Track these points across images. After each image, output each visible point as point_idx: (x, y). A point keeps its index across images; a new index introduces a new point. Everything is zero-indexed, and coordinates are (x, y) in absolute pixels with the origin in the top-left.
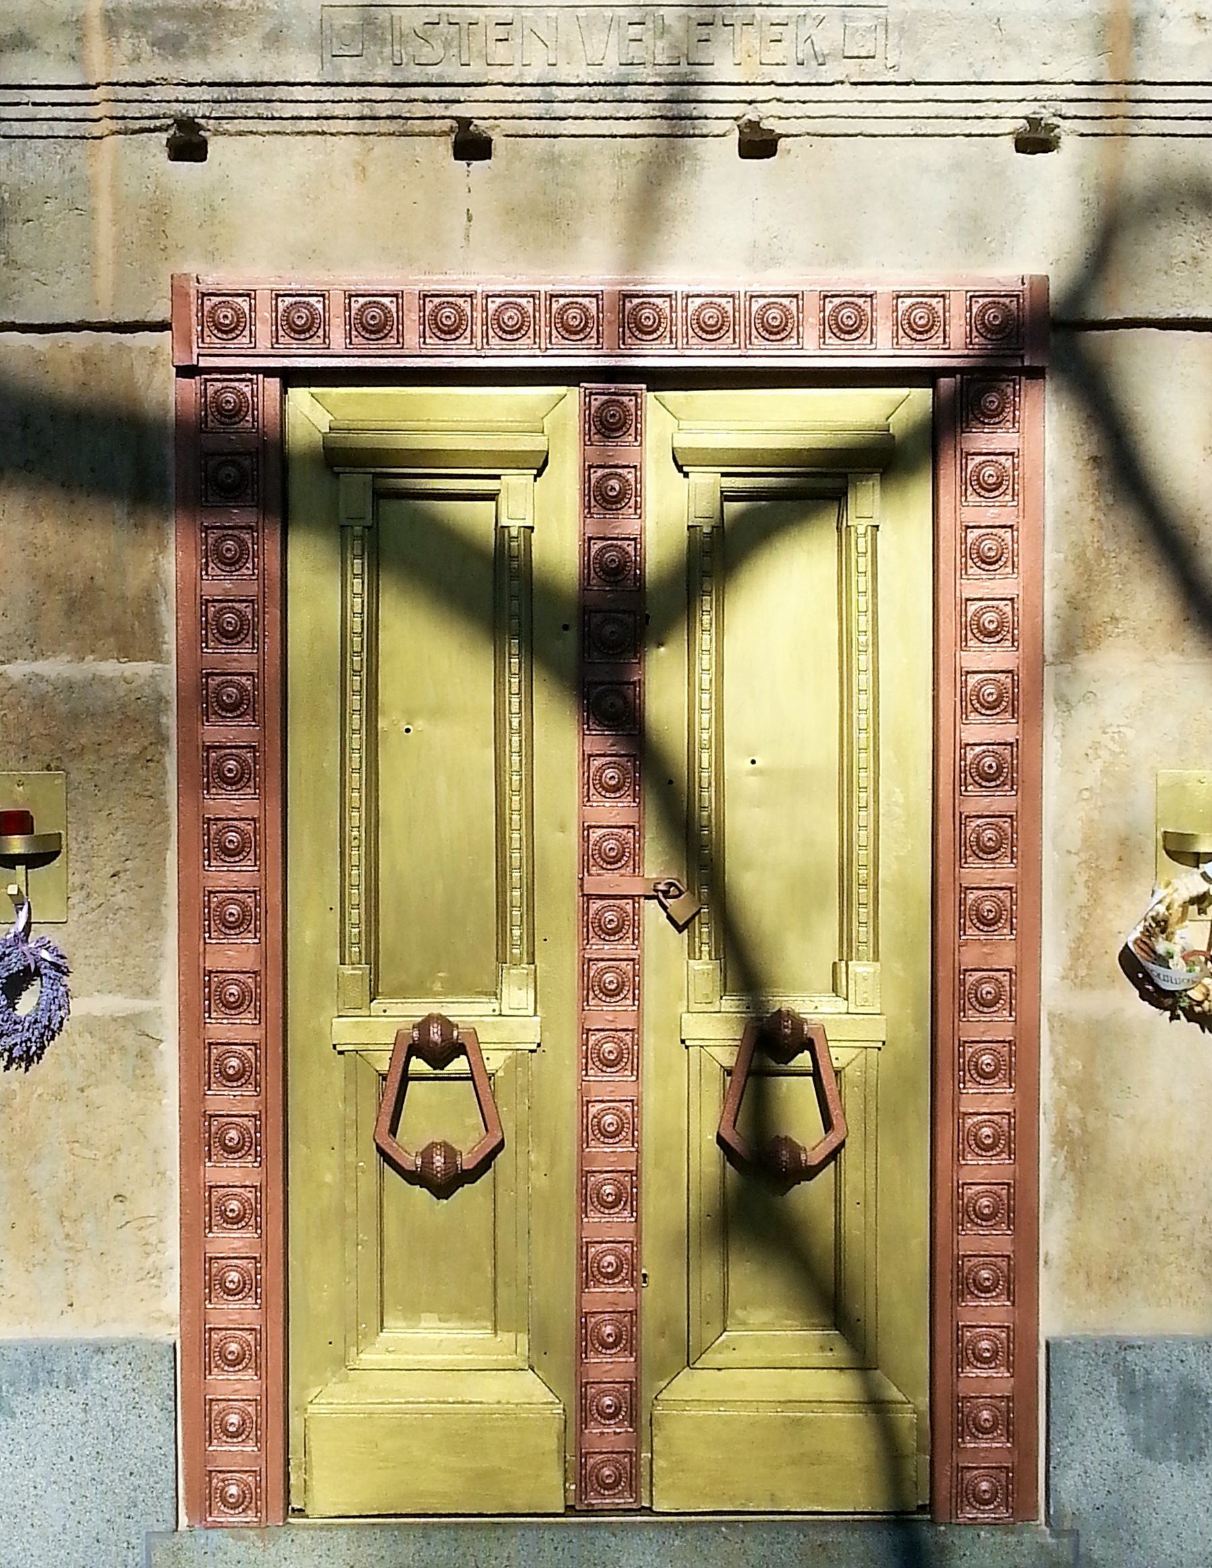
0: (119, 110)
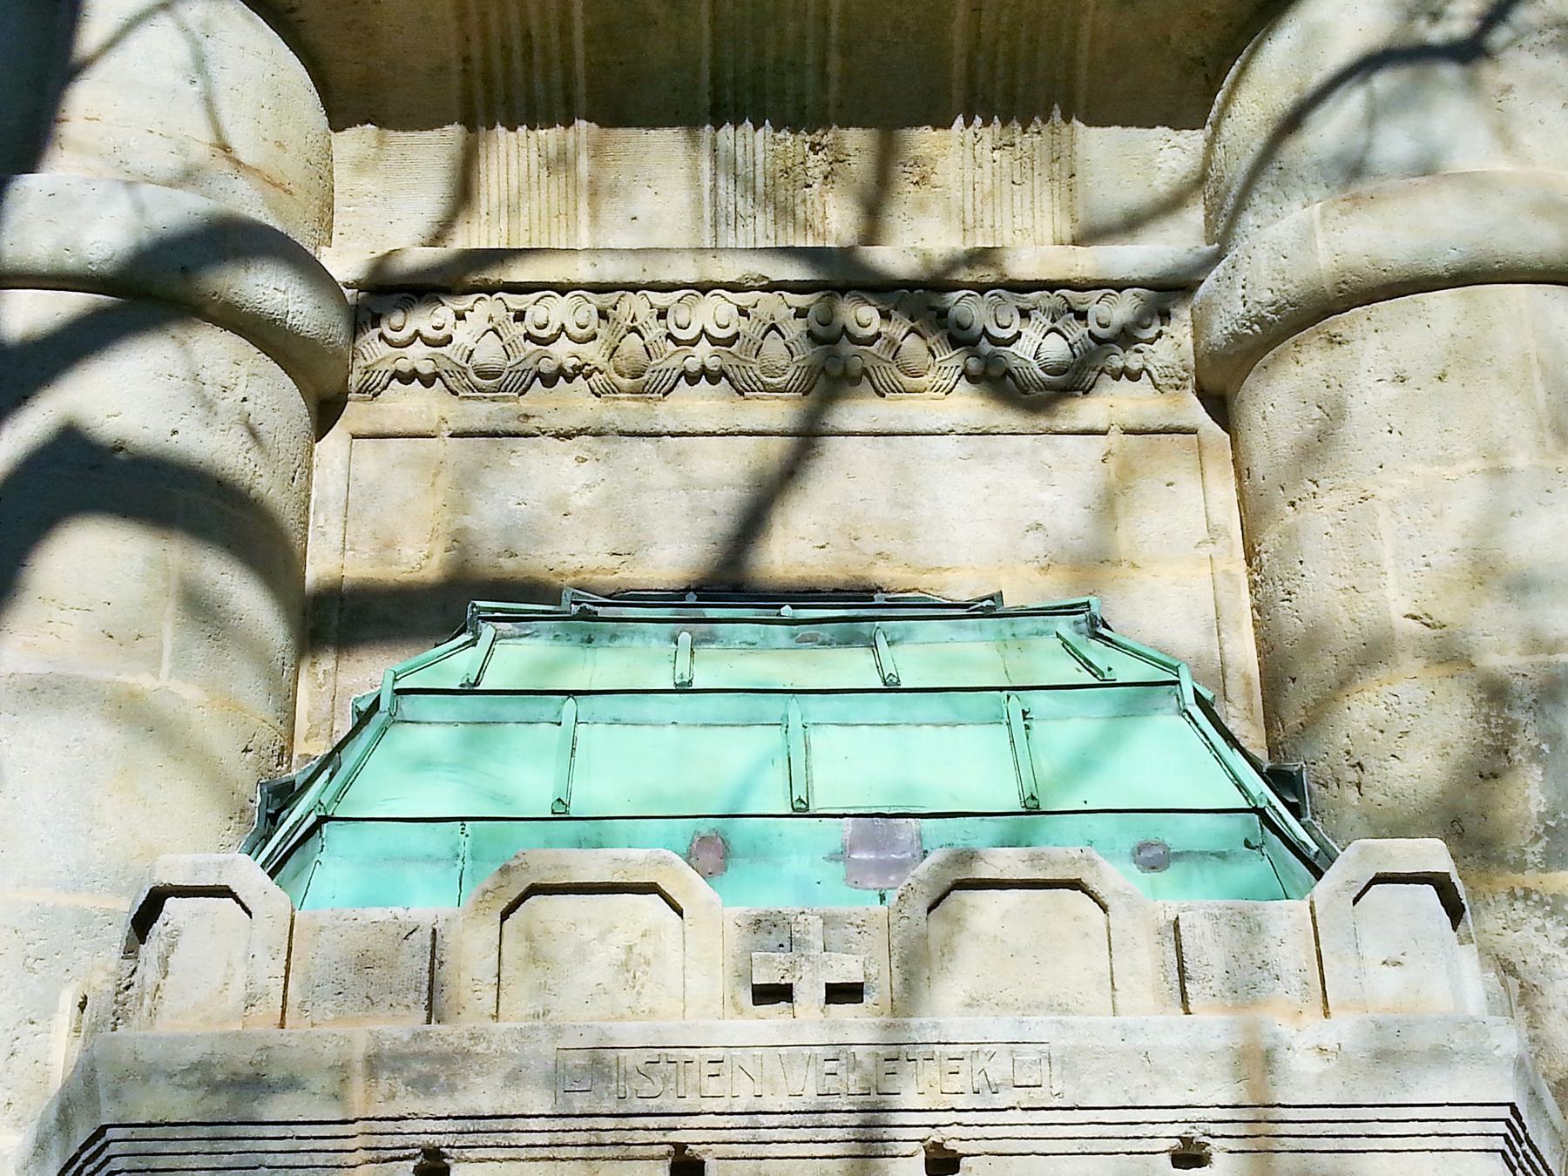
0: (374, 1141)
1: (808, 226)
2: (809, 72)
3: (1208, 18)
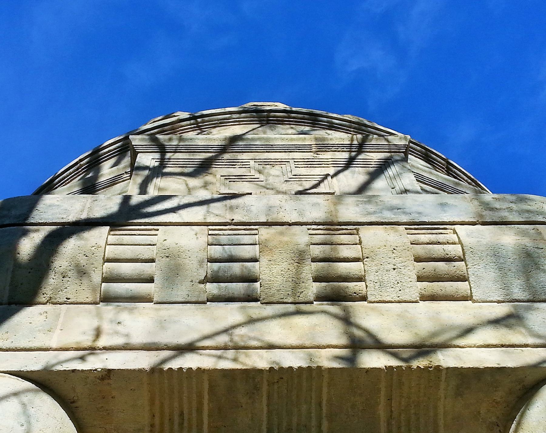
1: (148, 135)
2: (313, 429)
3: (497, 403)
